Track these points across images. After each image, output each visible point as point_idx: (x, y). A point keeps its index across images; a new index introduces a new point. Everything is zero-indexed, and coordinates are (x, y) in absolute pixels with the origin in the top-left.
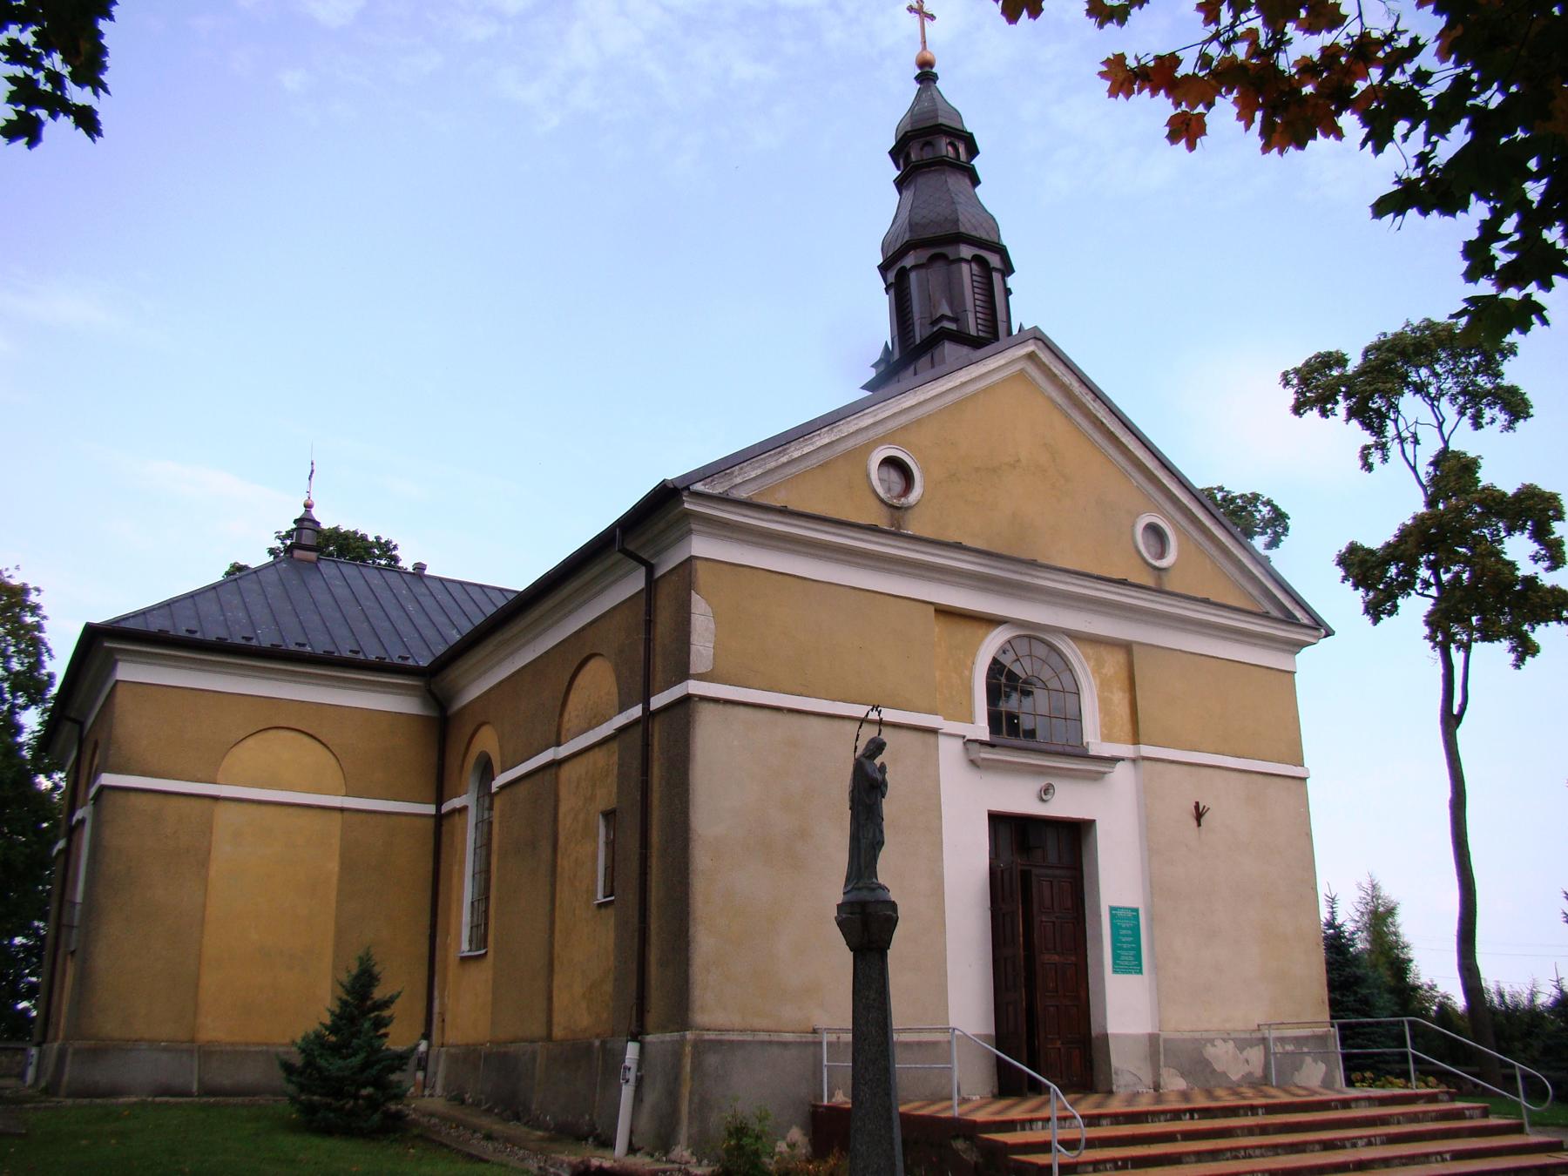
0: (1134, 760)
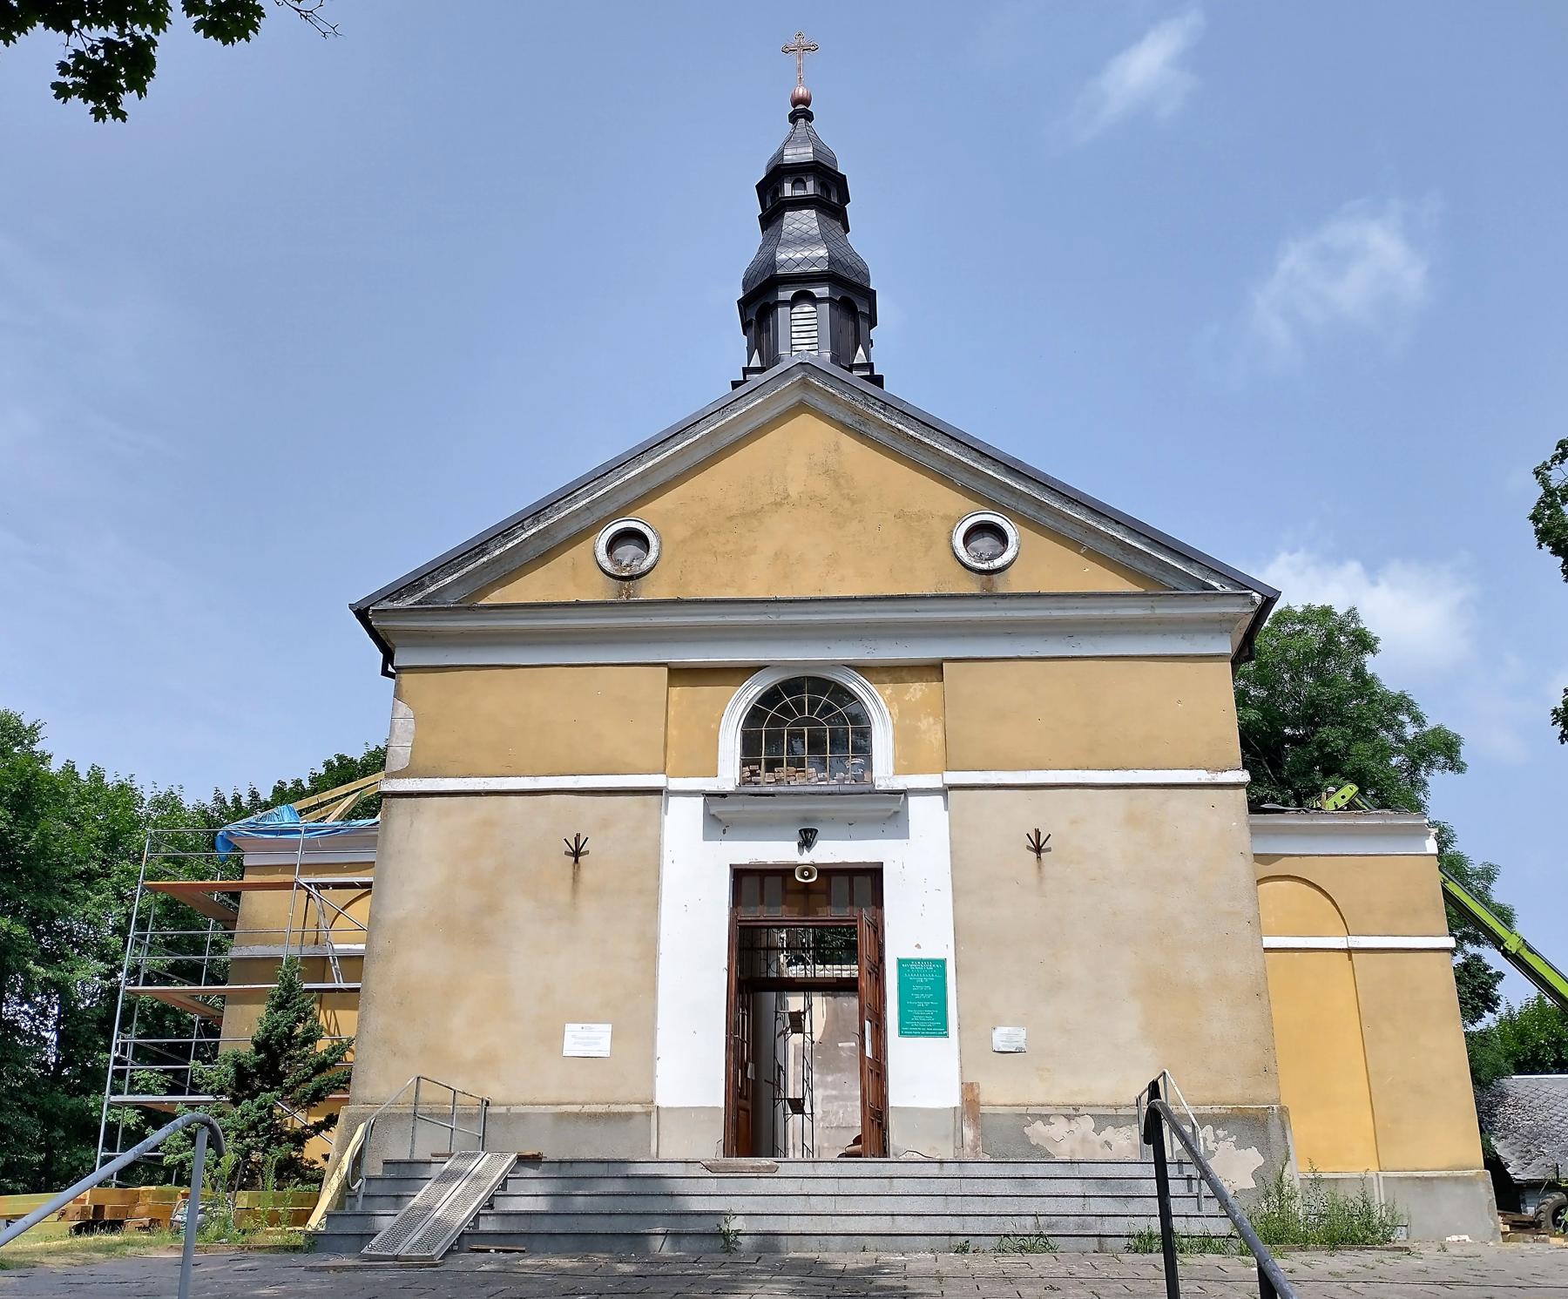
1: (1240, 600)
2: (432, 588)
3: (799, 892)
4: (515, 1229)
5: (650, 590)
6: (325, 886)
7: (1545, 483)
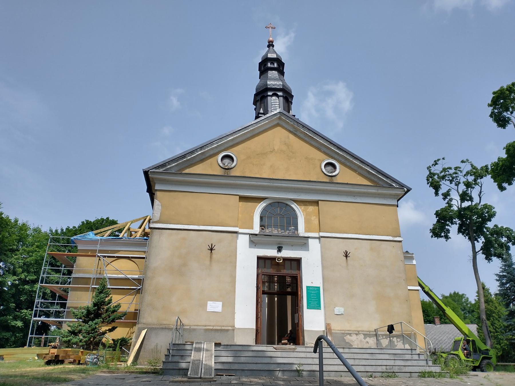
0: (319, 238)
1: (401, 190)
2: (169, 167)
3: (276, 265)
4: (225, 368)
5: (233, 173)
6: (105, 257)
7: (430, 171)
